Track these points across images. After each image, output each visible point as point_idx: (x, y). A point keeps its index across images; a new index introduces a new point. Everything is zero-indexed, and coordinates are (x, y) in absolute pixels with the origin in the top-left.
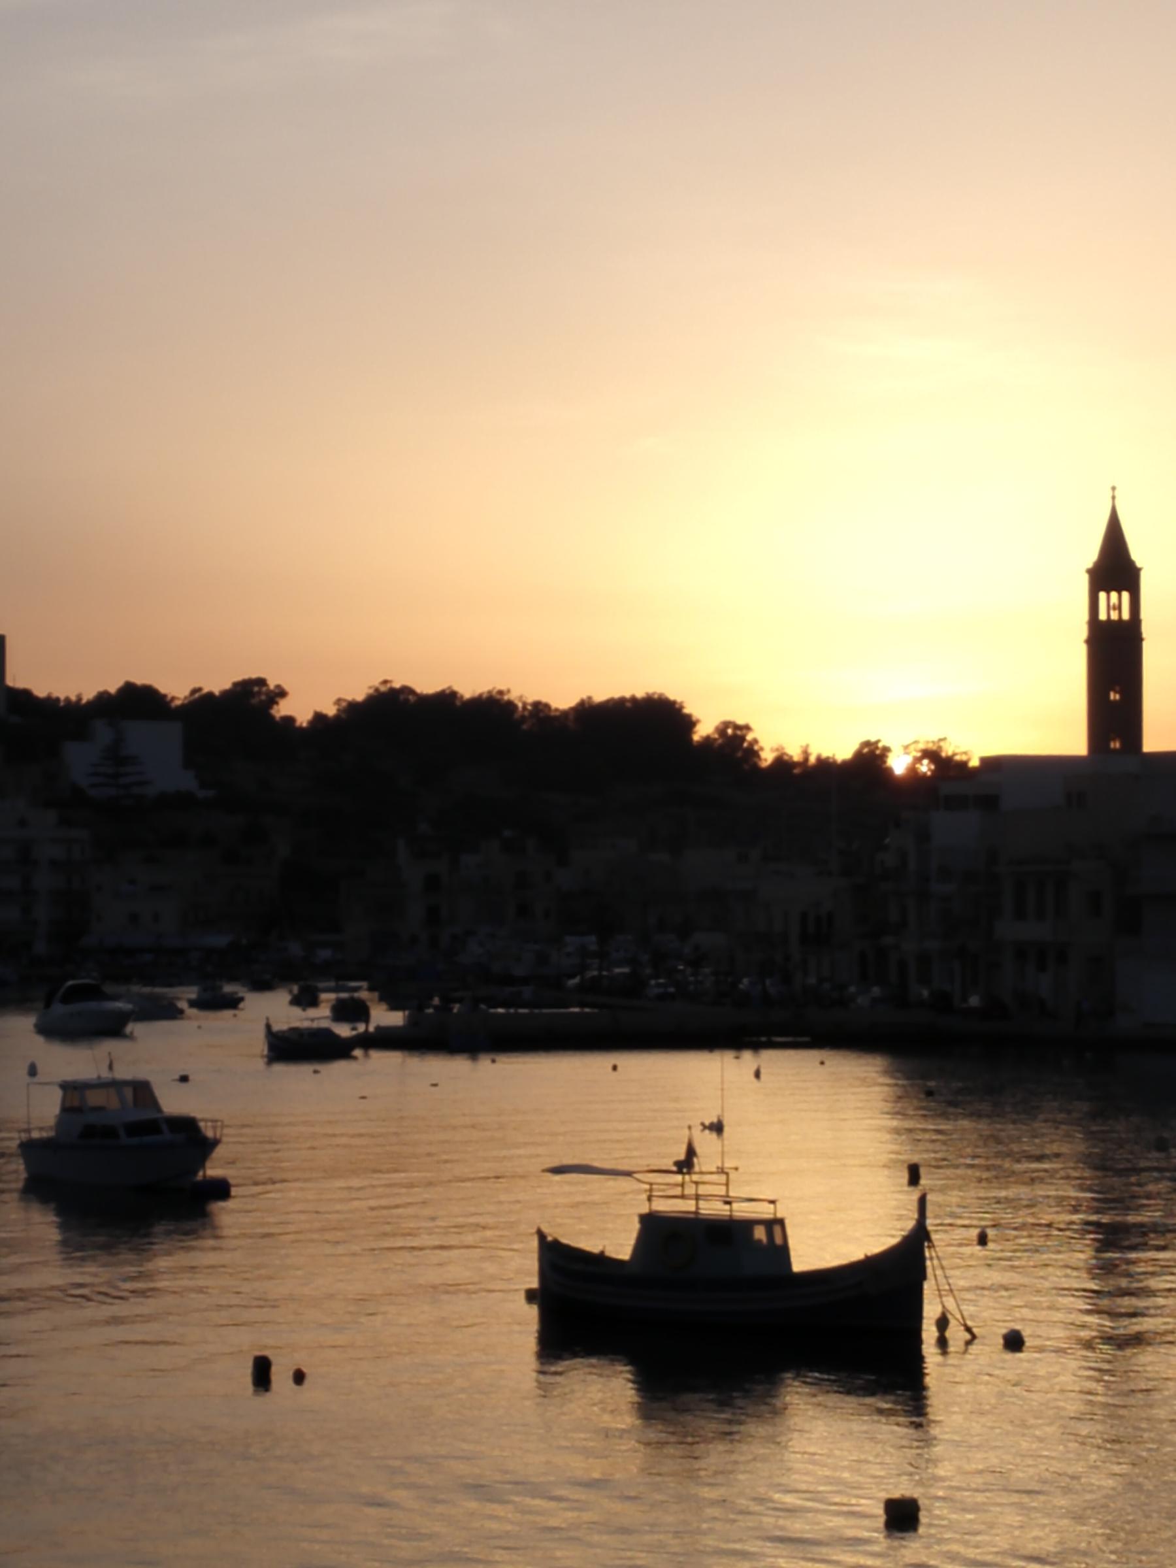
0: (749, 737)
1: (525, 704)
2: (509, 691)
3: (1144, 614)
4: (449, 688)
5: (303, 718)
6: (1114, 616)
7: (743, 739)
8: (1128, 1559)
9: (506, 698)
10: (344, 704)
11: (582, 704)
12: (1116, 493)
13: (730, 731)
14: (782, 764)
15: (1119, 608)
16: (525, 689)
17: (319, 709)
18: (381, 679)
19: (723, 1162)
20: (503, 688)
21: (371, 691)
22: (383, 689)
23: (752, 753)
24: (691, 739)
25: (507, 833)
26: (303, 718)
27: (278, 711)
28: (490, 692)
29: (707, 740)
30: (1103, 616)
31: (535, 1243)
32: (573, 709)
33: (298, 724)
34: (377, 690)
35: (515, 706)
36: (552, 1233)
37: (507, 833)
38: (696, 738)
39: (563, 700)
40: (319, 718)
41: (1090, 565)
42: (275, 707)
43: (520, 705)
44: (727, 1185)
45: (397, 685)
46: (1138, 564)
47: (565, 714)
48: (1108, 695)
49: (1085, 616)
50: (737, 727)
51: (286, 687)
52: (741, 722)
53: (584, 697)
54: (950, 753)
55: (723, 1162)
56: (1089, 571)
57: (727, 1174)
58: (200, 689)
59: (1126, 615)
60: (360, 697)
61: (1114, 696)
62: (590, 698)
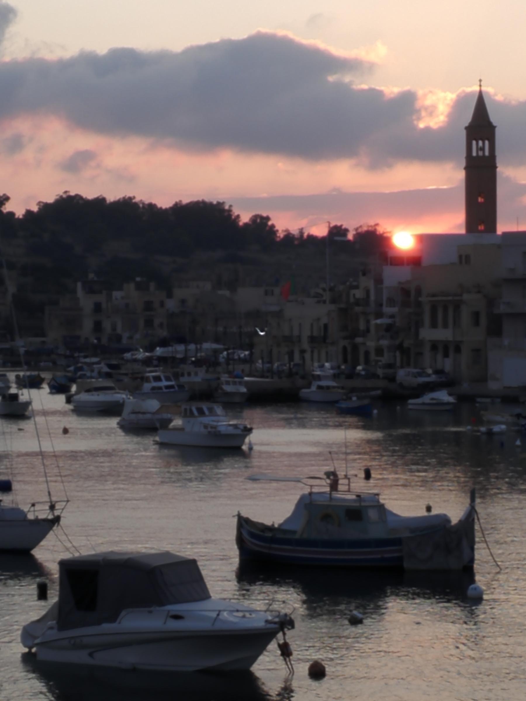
0: (270, 223)
1: (143, 204)
2: (134, 197)
3: (498, 153)
4: (101, 195)
5: (20, 213)
6: (481, 153)
7: (266, 224)
8: (54, 363)
9: (134, 201)
10: (42, 204)
11: (176, 204)
12: (482, 83)
13: (258, 221)
14: (289, 237)
15: (483, 149)
16: (142, 195)
17: (28, 208)
18: (63, 191)
19: (347, 472)
20: (131, 195)
21: (58, 197)
22: (64, 196)
23: (272, 230)
24: (238, 225)
25: (138, 279)
26: (20, 213)
27: (5, 209)
28: (124, 198)
29: (246, 224)
30: (474, 154)
31: (235, 520)
32: (171, 208)
33: (17, 216)
34: (61, 197)
35: (139, 207)
36: (244, 514)
37: (138, 279)
38: (241, 223)
39: (164, 203)
40: (29, 213)
41: (467, 124)
42: (4, 207)
43: (141, 205)
44: (349, 485)
45: (72, 193)
46: (495, 124)
47: (166, 210)
48: (477, 199)
49: (464, 154)
50: (262, 218)
51: (9, 194)
52: (265, 215)
53: (178, 200)
54: (381, 232)
55: (347, 472)
56: (466, 128)
57: (349, 479)
58: (69, 192)
59: (487, 153)
60: (50, 200)
61: (480, 200)
62: (181, 201)
